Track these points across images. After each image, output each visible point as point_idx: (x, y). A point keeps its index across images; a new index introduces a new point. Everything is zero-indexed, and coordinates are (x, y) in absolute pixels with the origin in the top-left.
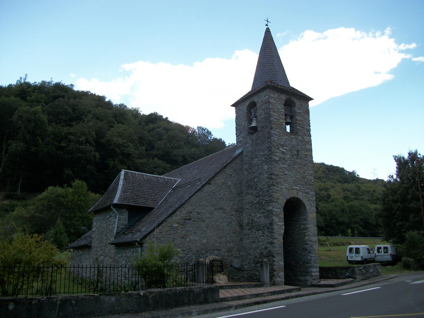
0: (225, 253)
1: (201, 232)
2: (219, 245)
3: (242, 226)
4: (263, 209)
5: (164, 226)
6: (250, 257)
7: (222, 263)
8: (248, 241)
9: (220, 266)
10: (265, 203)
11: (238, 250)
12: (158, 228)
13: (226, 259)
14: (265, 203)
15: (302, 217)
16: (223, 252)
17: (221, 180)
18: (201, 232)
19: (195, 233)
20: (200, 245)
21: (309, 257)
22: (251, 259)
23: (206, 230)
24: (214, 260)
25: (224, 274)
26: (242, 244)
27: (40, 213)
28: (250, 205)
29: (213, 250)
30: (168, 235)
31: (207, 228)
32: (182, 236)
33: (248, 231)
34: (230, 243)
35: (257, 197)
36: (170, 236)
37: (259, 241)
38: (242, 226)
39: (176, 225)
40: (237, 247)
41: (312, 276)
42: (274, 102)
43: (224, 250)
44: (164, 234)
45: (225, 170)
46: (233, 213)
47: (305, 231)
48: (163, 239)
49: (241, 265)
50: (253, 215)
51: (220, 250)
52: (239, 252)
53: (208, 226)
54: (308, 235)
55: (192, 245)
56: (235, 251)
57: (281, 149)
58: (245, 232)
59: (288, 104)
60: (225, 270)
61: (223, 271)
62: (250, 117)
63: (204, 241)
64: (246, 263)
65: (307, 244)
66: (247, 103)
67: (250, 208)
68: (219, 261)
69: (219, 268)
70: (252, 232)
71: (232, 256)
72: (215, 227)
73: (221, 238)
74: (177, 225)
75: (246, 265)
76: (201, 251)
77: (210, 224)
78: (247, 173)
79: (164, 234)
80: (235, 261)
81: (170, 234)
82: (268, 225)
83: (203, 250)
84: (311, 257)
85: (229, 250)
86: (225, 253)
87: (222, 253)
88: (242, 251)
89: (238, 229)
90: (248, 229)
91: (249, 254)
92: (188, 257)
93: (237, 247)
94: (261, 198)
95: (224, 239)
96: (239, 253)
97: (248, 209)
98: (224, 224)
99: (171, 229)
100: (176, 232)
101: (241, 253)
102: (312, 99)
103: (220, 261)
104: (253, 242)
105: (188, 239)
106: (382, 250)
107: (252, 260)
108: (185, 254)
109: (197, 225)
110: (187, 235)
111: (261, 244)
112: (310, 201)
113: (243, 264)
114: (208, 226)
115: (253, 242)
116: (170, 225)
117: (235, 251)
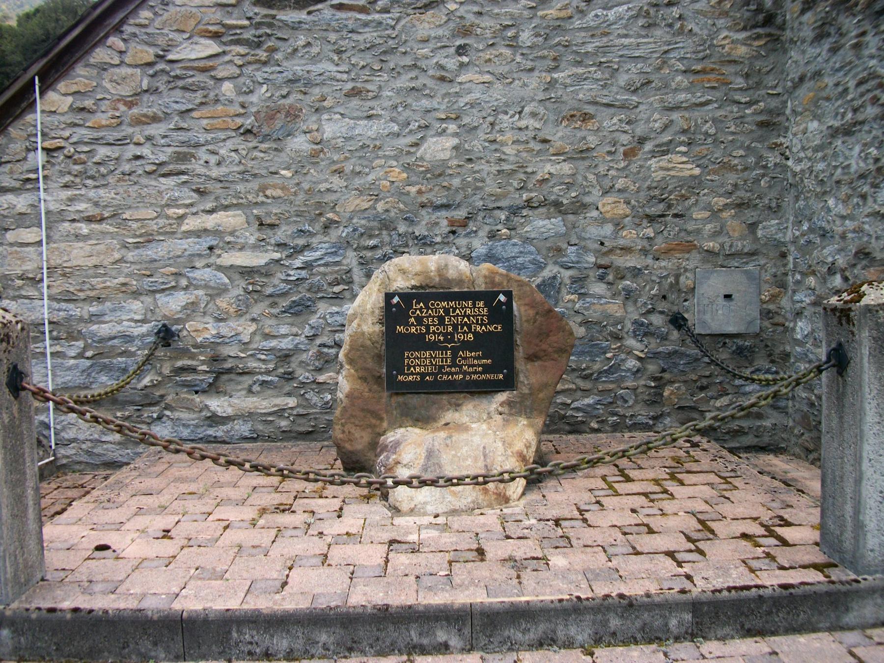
0: (618, 225)
1: (403, 82)
2: (567, 168)
3: (769, 20)
5: (103, 67)
6: (828, 253)
7: (501, 313)
8: (814, 125)
9: (481, 342)
11: (741, 206)
13: (636, 272)
16: (602, 221)
18: (403, 82)
19: (355, 93)
20: (398, 174)
22: (832, 271)
23: (451, 63)
24: (424, 294)
25: (515, 409)
26: (773, 158)
27: (556, 81)
29: (514, 211)
30: (138, 122)
31: (461, 50)
32: (249, 122)
33: (812, 51)
34: (664, 150)
36: (155, 130)
38: (769, 20)
40: (732, 178)
44: (102, 119)
48: (103, 152)
49: (767, 314)
51: (579, 207)
52: (751, 215)
53: (466, 31)
55: (337, 182)
56: (715, 214)
58: (798, 60)
60: (529, 375)
61: (509, 384)
63: (438, 148)
64: (804, 298)
68: (474, 296)
69: (473, 364)
70: (834, 50)
71: (689, 247)
72: (526, 37)
73: (586, 117)
74: (211, 47)
75: (799, 314)
76: (409, 221)
77: (486, 22)
79: (102, 119)
80: (714, 284)
81: (155, 119)
83: (426, 216)
85: (662, 207)
86: (618, 225)
87: (594, 232)
88: (775, 210)
89: (735, 42)
90: (808, 33)
91: (824, 234)
92: (307, 266)
93: (732, 178)
95: (610, 121)
96: (753, 227)
98: (611, 14)
99: (161, 83)
100: (198, 97)
101: (770, 227)
103: (488, 297)
104: (847, 131)
105: (300, 143)
107: (837, 281)
108: (281, 246)
109: (369, 35)
110: (293, 114)
113: (785, 302)
114: (466, 31)
116: (149, 54)
117: (715, 214)
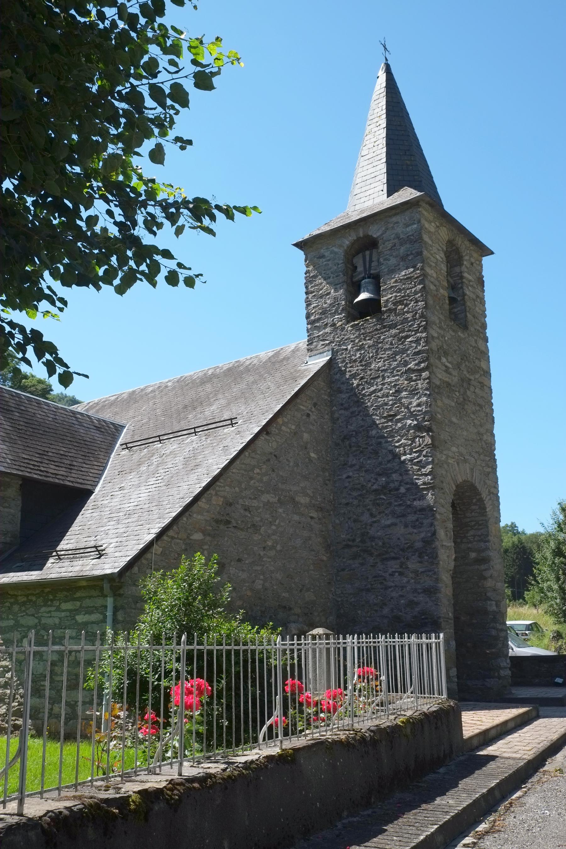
4: (400, 505)
5: (172, 538)
10: (408, 490)
12: (159, 543)
14: (408, 490)
15: (471, 533)
17: (290, 425)
21: (494, 633)
23: (262, 553)
28: (355, 494)
33: (351, 562)
34: (308, 590)
35: (380, 475)
37: (386, 588)
39: (197, 536)
41: (499, 677)
42: (430, 243)
43: (297, 610)
45: (298, 401)
46: (314, 514)
47: (482, 567)
50: (366, 518)
54: (491, 576)
57: (444, 360)
59: (454, 257)
62: (352, 277)
63: (258, 585)
65: (489, 599)
66: (352, 237)
67: (356, 502)
78: (347, 413)
82: (419, 545)
84: (497, 630)
94: (395, 476)
97: (347, 504)
102: (492, 253)
106: (257, 642)
111: (394, 594)
112: (492, 495)
115: (368, 590)
